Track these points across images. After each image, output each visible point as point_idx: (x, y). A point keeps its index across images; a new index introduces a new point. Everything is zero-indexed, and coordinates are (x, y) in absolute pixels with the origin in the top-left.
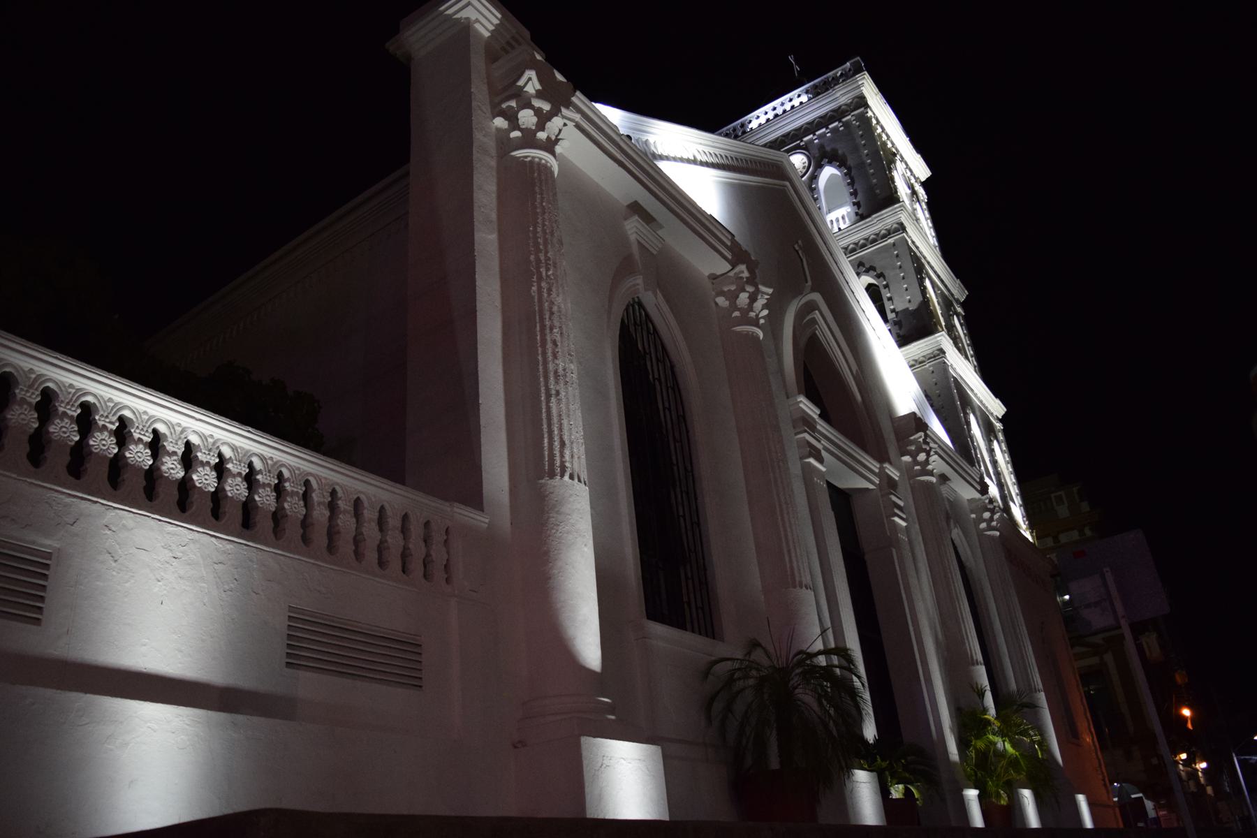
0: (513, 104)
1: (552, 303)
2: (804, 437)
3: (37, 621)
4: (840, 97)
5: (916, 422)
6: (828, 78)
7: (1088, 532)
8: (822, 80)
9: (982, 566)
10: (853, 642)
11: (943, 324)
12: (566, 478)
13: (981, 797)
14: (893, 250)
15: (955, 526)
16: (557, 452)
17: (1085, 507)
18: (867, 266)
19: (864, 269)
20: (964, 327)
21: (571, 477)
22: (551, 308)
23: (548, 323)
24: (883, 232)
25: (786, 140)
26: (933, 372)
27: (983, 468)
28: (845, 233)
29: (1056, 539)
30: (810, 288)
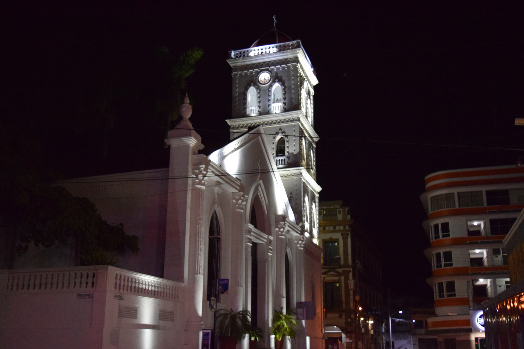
0: (197, 171)
1: (201, 230)
2: (248, 237)
3: (136, 318)
4: (288, 55)
5: (284, 218)
6: (286, 44)
7: (347, 228)
8: (283, 44)
9: (295, 259)
10: (249, 309)
11: (305, 157)
12: (200, 275)
13: (275, 338)
14: (293, 127)
15: (288, 248)
16: (199, 269)
17: (349, 217)
18: (283, 131)
19: (281, 132)
20: (314, 153)
21: (201, 275)
22: (201, 232)
23: (200, 236)
24: (291, 119)
25: (264, 65)
26: (296, 181)
27: (305, 218)
28: (277, 115)
29: (334, 228)
30: (259, 178)
